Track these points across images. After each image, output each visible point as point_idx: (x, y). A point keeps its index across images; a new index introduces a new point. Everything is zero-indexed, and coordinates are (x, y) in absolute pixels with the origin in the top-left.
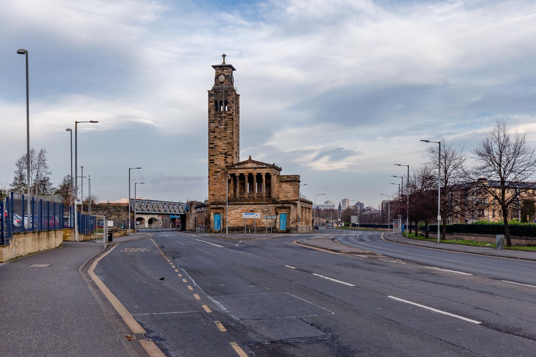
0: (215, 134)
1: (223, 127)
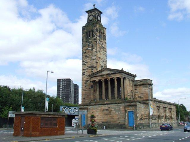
0: (86, 54)
1: (90, 48)
